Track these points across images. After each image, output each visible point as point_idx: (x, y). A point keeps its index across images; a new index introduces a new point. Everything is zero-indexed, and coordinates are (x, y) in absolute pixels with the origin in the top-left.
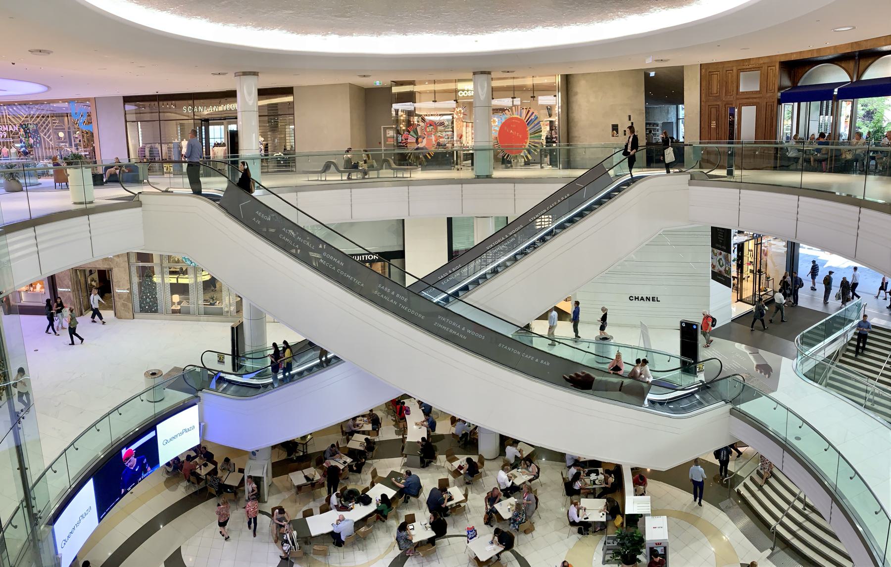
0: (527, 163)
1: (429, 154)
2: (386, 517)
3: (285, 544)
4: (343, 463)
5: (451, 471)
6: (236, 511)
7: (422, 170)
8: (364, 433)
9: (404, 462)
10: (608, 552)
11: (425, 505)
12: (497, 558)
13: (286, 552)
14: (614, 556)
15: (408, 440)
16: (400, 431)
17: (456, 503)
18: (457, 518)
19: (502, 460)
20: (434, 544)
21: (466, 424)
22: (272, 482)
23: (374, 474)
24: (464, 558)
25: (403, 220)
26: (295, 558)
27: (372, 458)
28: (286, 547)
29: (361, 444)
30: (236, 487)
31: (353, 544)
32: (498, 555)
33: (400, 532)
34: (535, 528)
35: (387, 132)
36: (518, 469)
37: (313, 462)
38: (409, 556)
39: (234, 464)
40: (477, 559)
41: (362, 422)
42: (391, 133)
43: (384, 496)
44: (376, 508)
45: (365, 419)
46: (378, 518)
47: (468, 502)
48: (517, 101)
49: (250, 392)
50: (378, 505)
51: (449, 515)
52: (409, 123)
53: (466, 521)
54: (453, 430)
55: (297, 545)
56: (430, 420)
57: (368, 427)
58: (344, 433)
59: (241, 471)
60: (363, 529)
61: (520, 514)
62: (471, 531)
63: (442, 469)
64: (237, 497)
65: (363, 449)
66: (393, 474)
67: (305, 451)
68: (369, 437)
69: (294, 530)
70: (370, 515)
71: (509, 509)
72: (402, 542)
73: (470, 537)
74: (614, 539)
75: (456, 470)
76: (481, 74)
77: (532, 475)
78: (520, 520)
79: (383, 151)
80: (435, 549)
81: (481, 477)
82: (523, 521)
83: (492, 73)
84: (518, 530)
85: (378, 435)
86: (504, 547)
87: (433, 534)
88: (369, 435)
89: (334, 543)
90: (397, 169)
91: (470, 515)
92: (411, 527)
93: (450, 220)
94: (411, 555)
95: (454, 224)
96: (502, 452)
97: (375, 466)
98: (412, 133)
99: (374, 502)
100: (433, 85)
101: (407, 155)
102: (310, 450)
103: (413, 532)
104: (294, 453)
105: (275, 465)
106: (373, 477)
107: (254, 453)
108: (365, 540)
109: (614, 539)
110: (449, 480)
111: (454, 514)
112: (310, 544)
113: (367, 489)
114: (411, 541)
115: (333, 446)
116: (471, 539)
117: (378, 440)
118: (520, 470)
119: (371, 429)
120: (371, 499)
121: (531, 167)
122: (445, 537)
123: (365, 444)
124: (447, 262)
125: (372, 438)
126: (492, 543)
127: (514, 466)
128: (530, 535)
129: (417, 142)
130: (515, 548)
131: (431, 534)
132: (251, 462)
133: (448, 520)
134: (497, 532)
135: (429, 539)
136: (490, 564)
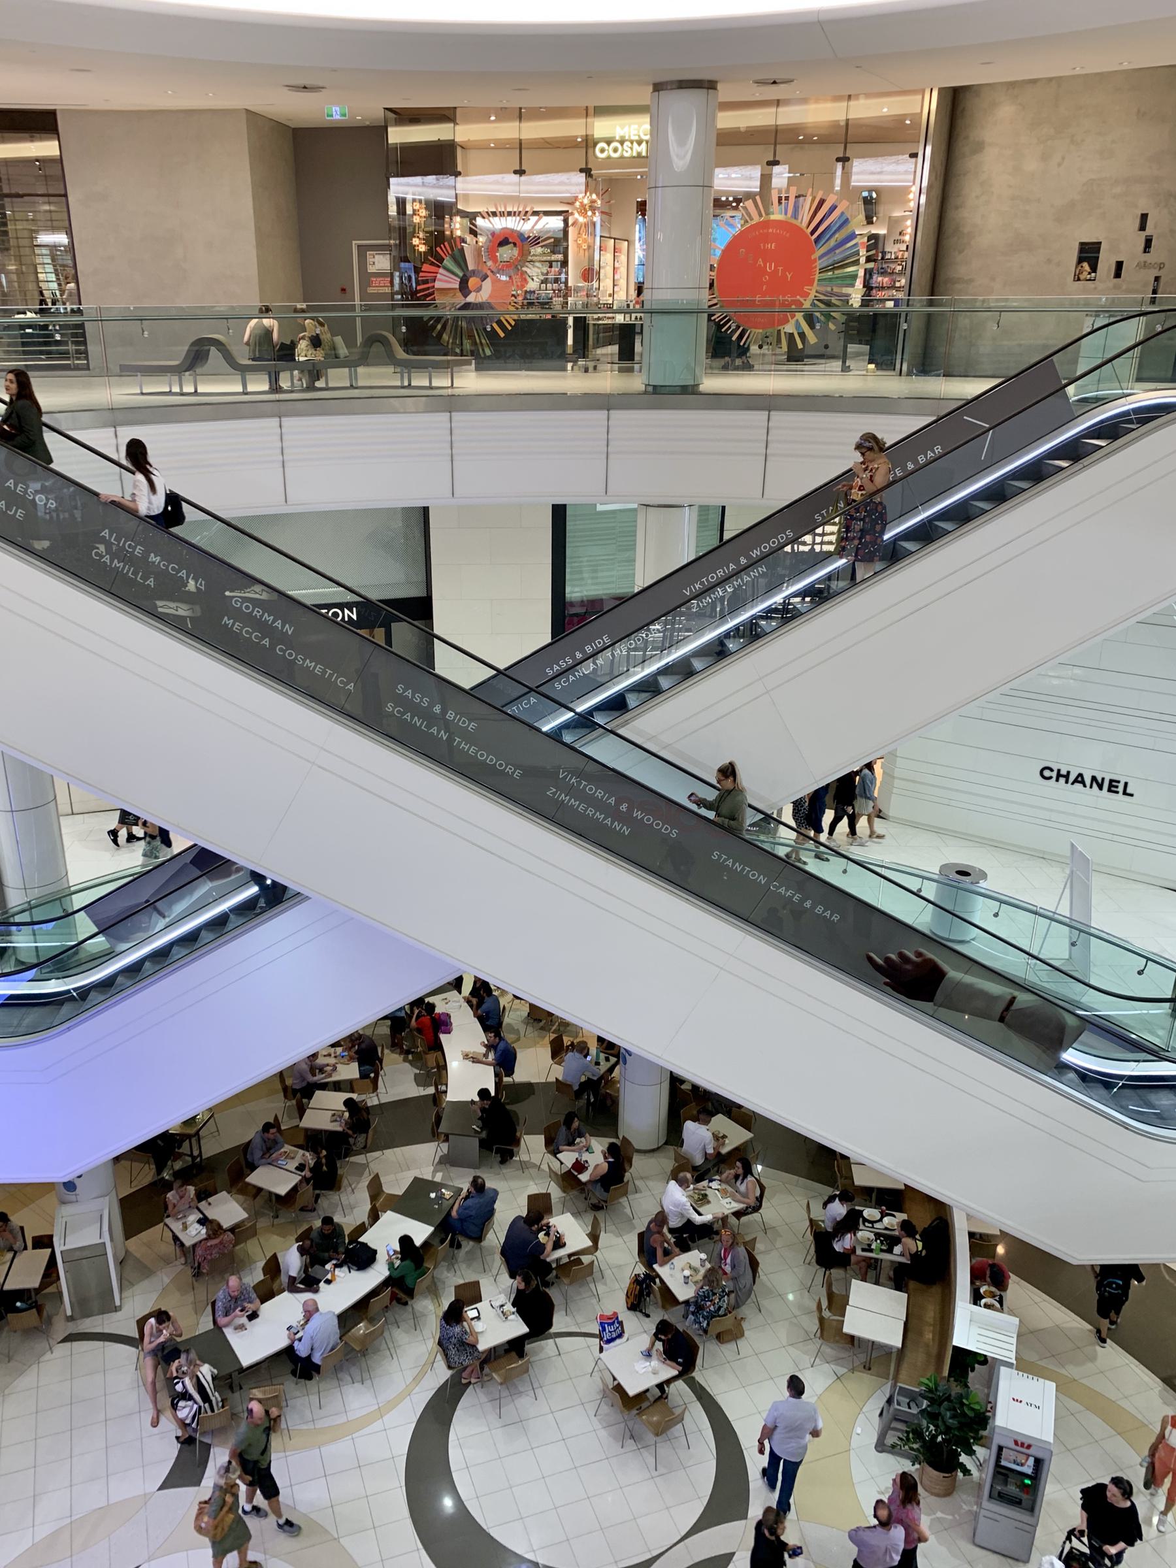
0: (796, 356)
1: (500, 323)
2: (410, 1293)
3: (182, 1404)
4: (297, 1168)
5: (556, 1174)
6: (48, 1356)
7: (477, 369)
8: (337, 1086)
9: (440, 1153)
10: (895, 1424)
11: (498, 1261)
12: (657, 1392)
13: (188, 1421)
14: (908, 1439)
15: (452, 1096)
16: (428, 1074)
17: (570, 1256)
18: (571, 1290)
19: (672, 1154)
20: (521, 1354)
21: (589, 1058)
22: (127, 1252)
23: (375, 1189)
24: (590, 1388)
25: (426, 510)
26: (213, 1433)
27: (366, 1149)
28: (186, 1411)
29: (336, 1117)
30: (35, 1289)
31: (337, 1369)
32: (660, 1386)
33: (448, 1324)
34: (746, 1333)
35: (370, 260)
36: (711, 1181)
37: (222, 1177)
38: (470, 1383)
39: (22, 1228)
40: (619, 1389)
41: (332, 1061)
42: (381, 263)
43: (406, 1241)
44: (387, 1273)
45: (339, 1050)
46: (394, 1297)
47: (598, 1253)
48: (781, 176)
49: (26, 1022)
50: (391, 1265)
51: (553, 1283)
52: (437, 239)
53: (594, 1301)
54: (557, 1072)
55: (215, 1397)
56: (502, 1046)
57: (350, 1071)
58: (288, 1092)
59: (43, 1242)
60: (362, 1328)
61: (714, 1294)
62: (609, 1324)
63: (533, 1171)
64: (45, 1313)
65: (340, 1129)
66: (420, 1187)
67: (196, 1153)
68: (354, 1096)
69: (204, 1362)
70: (374, 1293)
71: (686, 1278)
72: (452, 1352)
73: (606, 1336)
74: (913, 1398)
75: (569, 1171)
76: (681, 88)
77: (744, 1203)
78: (712, 1308)
79: (358, 309)
80: (529, 1362)
81: (625, 1194)
82: (721, 1312)
83: (719, 86)
84: (706, 1331)
85: (375, 1088)
86: (681, 1368)
87: (523, 1329)
88: (353, 1092)
89: (294, 1373)
90: (409, 366)
91: (605, 1284)
92: (472, 1314)
93: (559, 513)
94: (473, 1381)
95: (572, 526)
96: (674, 1134)
97: (375, 1167)
98: (448, 262)
99: (382, 1258)
100: (523, 137)
101: (434, 327)
102: (210, 1149)
103: (478, 1326)
104: (169, 1163)
105: (126, 1204)
106: (374, 1198)
107: (70, 1186)
108: (364, 1356)
109: (913, 1398)
110: (552, 1197)
111: (566, 1281)
112: (241, 1388)
113: (362, 1229)
114: (474, 1347)
115: (267, 1127)
116: (609, 1341)
117: (376, 1102)
118: (715, 1185)
119: (357, 1076)
120: (375, 1252)
121: (806, 368)
122: (547, 1338)
123: (347, 1115)
124: (549, 640)
125: (363, 1097)
126: (648, 1355)
127: (701, 1174)
128: (731, 1346)
129: (464, 288)
130: (697, 1375)
131: (518, 1327)
132: (66, 1210)
133: (554, 1293)
134: (663, 1329)
135: (510, 1342)
136: (645, 1405)
